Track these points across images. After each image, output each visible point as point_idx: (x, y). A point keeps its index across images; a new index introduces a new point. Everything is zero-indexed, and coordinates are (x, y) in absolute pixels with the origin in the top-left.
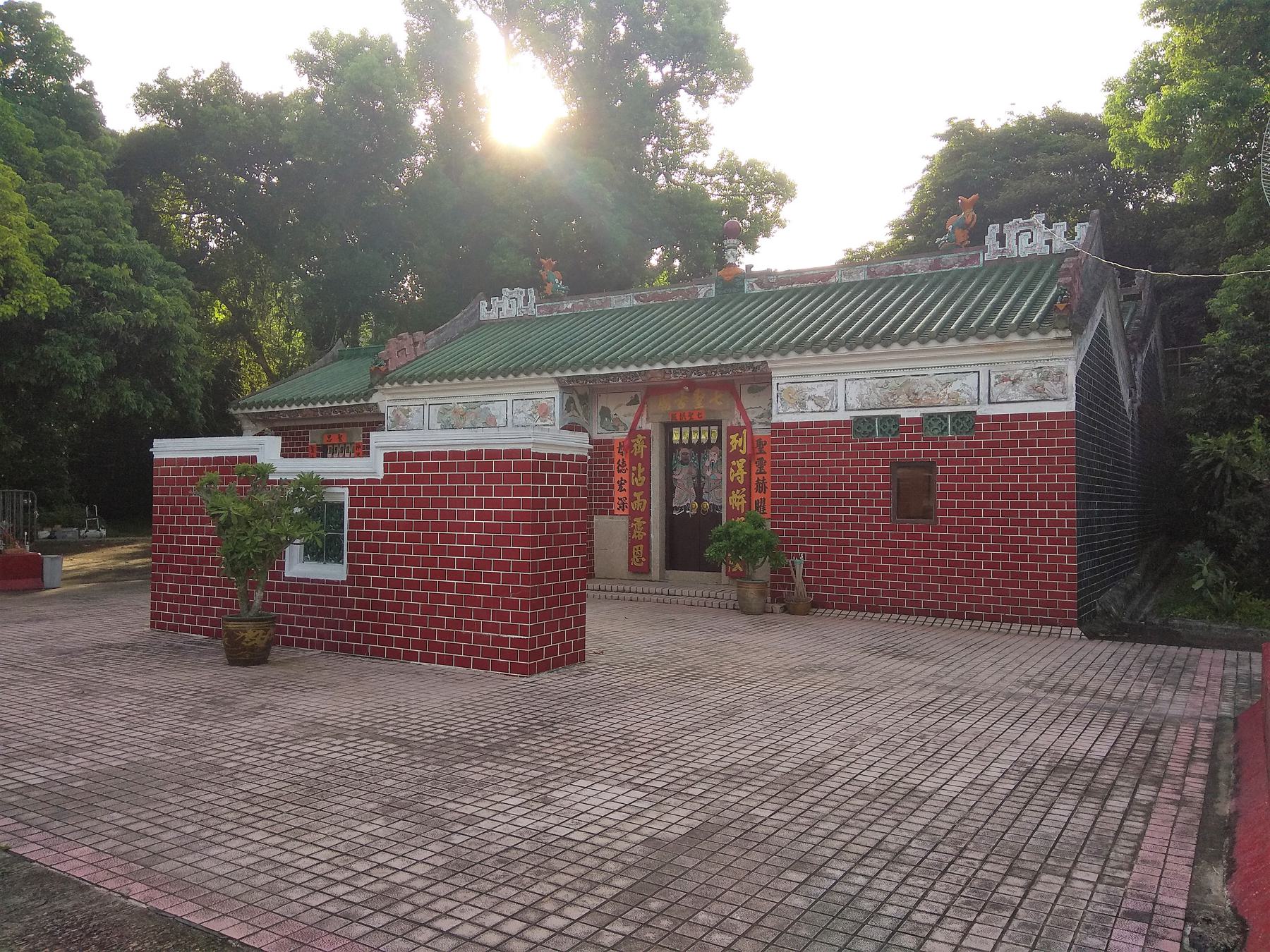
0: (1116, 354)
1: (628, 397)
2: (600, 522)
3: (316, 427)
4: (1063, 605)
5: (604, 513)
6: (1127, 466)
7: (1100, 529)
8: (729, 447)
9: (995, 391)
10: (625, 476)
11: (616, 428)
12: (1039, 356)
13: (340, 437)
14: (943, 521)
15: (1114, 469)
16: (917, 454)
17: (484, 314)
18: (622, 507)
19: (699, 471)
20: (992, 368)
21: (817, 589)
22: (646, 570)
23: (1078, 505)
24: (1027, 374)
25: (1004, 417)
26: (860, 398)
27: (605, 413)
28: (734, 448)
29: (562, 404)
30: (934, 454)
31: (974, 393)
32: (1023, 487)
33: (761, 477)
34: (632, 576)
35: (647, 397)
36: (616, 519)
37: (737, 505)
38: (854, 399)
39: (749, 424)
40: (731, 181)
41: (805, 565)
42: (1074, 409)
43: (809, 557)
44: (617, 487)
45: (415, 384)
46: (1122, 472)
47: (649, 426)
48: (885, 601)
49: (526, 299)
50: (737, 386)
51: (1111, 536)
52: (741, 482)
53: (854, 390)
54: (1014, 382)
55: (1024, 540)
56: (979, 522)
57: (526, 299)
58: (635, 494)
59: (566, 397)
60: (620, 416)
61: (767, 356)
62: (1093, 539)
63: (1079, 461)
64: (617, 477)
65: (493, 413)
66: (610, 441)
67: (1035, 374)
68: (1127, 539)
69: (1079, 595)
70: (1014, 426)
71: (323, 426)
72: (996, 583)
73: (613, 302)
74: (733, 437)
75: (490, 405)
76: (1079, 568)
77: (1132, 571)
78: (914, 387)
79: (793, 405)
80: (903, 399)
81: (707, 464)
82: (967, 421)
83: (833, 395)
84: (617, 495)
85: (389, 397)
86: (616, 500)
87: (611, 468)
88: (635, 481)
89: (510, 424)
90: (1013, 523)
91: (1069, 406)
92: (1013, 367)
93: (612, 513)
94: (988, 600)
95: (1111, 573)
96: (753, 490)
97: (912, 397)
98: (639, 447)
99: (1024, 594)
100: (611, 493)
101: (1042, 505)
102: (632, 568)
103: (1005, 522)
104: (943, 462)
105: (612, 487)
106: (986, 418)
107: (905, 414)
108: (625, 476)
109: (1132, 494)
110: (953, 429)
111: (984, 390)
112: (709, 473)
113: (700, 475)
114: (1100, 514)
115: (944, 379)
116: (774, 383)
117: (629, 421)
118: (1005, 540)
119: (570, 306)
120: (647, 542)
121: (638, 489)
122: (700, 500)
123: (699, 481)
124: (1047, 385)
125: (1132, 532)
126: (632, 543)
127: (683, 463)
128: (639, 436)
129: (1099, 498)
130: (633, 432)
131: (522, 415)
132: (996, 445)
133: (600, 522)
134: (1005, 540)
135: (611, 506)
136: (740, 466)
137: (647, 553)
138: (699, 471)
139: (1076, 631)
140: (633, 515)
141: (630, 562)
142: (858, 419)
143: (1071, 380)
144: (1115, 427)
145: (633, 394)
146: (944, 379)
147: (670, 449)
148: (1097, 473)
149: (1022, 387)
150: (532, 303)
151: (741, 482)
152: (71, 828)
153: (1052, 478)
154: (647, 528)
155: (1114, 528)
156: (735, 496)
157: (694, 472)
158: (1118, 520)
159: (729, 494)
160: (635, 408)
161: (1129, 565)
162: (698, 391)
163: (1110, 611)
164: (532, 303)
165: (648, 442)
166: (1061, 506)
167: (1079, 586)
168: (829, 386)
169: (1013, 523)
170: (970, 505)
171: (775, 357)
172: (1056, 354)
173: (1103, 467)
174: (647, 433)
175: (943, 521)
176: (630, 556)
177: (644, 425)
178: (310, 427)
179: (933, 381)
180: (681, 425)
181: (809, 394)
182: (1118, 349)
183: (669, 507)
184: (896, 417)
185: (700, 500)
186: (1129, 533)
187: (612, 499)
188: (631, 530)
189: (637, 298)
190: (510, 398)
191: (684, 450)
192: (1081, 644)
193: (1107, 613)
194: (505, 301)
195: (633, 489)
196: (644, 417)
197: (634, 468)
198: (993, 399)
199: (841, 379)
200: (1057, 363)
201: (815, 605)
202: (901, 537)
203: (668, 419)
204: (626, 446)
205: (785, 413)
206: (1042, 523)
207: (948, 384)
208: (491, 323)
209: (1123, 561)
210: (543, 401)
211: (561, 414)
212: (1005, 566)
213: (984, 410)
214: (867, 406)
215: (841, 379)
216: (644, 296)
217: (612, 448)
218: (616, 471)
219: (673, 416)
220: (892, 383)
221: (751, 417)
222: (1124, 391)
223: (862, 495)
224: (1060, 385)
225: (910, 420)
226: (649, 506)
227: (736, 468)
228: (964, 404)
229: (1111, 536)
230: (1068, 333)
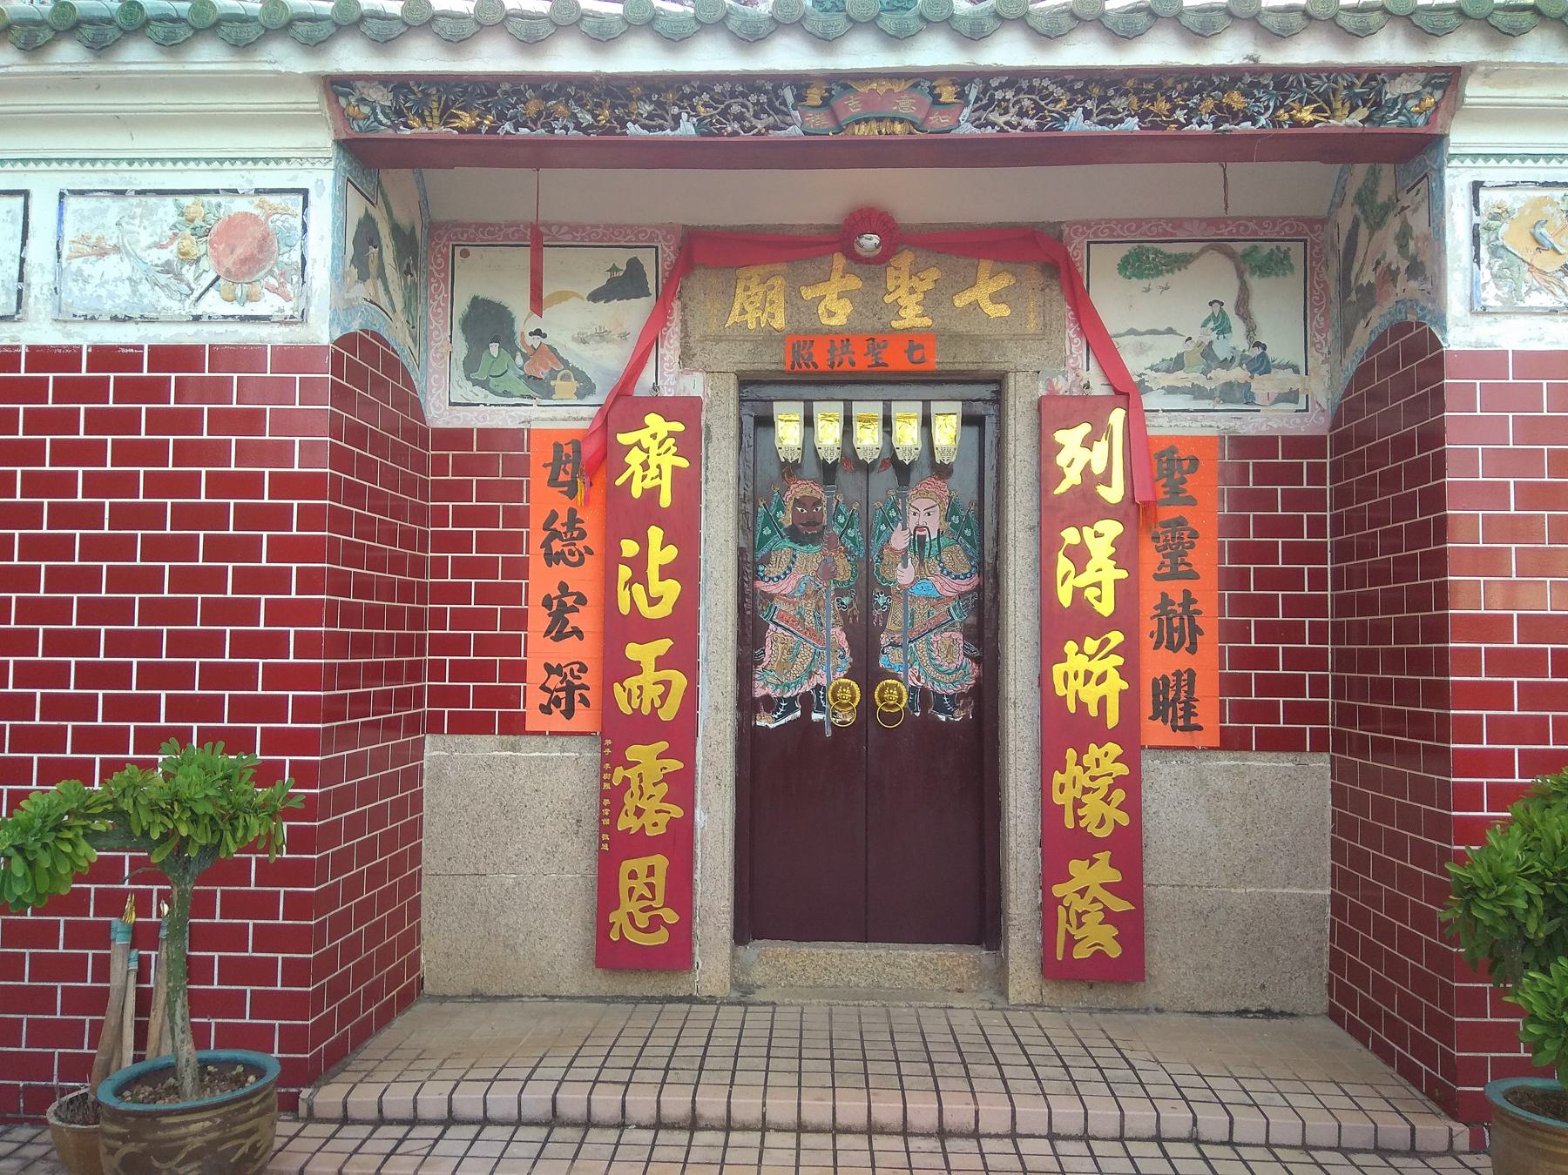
1: (596, 268)
8: (1047, 472)
10: (583, 579)
11: (540, 387)
18: (565, 699)
22: (677, 954)
27: (487, 323)
28: (1073, 478)
33: (1175, 590)
34: (602, 983)
36: (529, 751)
37: (1091, 695)
39: (1126, 393)
44: (539, 619)
47: (694, 385)
50: (1076, 249)
52: (1106, 608)
58: (633, 651)
64: (541, 581)
66: (513, 437)
74: (1070, 439)
81: (900, 540)
84: (539, 650)
86: (536, 674)
87: (513, 543)
93: (514, 726)
96: (1147, 642)
102: (611, 954)
105: (519, 620)
108: (583, 579)
112: (905, 575)
116: (1456, 181)
120: (679, 843)
121: (647, 630)
122: (867, 671)
123: (869, 602)
126: (615, 848)
127: (795, 535)
128: (654, 421)
131: (113, 266)
137: (681, 889)
140: (620, 732)
141: (603, 926)
145: (621, 258)
147: (763, 479)
151: (1106, 608)
154: (682, 787)
156: (1075, 659)
157: (844, 569)
160: (633, 313)
162: (905, 259)
174: (684, 409)
176: (606, 896)
177: (668, 376)
183: (747, 704)
185: (867, 671)
188: (613, 798)
196: (670, 351)
197: (629, 548)
203: (771, 360)
205: (1513, 310)
210: (240, 205)
217: (520, 466)
221: (1135, 364)
223: (152, 612)
227: (1080, 556)
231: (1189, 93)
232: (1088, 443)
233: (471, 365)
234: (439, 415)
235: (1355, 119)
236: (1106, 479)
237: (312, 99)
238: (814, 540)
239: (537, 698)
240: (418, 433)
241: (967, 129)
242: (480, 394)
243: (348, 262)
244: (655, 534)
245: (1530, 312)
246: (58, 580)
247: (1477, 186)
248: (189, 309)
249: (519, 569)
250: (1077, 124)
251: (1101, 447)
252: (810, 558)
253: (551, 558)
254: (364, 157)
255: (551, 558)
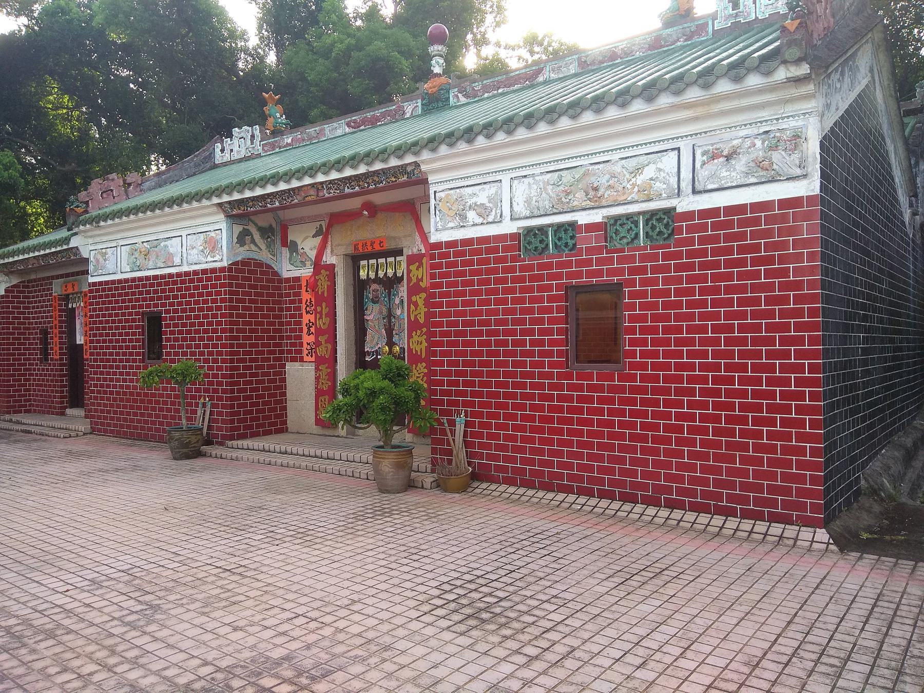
0: (890, 147)
1: (312, 228)
2: (292, 368)
3: (58, 277)
4: (801, 493)
5: (294, 360)
6: (908, 300)
7: (867, 373)
9: (702, 174)
11: (303, 264)
12: (765, 114)
13: (73, 286)
14: (633, 366)
15: (889, 294)
16: (599, 273)
17: (219, 158)
19: (389, 310)
20: (698, 141)
21: (481, 456)
23: (824, 340)
24: (748, 143)
25: (714, 212)
26: (528, 201)
28: (414, 280)
29: (230, 237)
30: (620, 272)
31: (673, 181)
32: (742, 315)
35: (329, 226)
38: (521, 205)
40: (532, 53)
41: (467, 424)
42: (817, 191)
43: (474, 414)
44: (305, 329)
45: (102, 223)
46: (900, 297)
48: (560, 476)
49: (253, 136)
50: (417, 206)
51: (885, 379)
52: (422, 321)
53: (522, 190)
54: (728, 158)
55: (743, 394)
56: (680, 367)
57: (253, 136)
59: (238, 229)
60: (307, 250)
61: (416, 154)
62: (854, 387)
63: (825, 272)
64: (306, 318)
65: (171, 250)
67: (758, 143)
68: (908, 381)
69: (826, 478)
70: (728, 224)
71: (61, 276)
72: (704, 456)
73: (327, 132)
75: (169, 243)
76: (827, 437)
77: (914, 418)
78: (593, 179)
79: (453, 218)
80: (579, 198)
81: (397, 301)
82: (664, 220)
83: (496, 200)
85: (91, 241)
86: (305, 345)
87: (299, 309)
88: (320, 323)
89: (185, 262)
90: (728, 367)
91: (810, 187)
92: (727, 136)
93: (302, 360)
94: (694, 481)
95: (883, 429)
97: (592, 193)
98: (323, 285)
99: (744, 473)
100: (300, 337)
101: (770, 341)
102: (319, 422)
103: (717, 368)
104: (632, 283)
105: (301, 330)
106: (689, 215)
107: (583, 218)
109: (915, 326)
110: (647, 235)
111: (686, 174)
113: (390, 315)
114: (865, 351)
115: (632, 163)
117: (312, 254)
118: (716, 393)
119: (289, 141)
123: (390, 322)
124: (776, 156)
125: (915, 371)
127: (374, 302)
129: (867, 330)
130: (318, 265)
131: (195, 251)
132: (703, 253)
133: (292, 368)
134: (716, 393)
135: (300, 352)
136: (421, 303)
138: (389, 310)
139: (822, 535)
140: (319, 361)
141: (316, 415)
142: (529, 231)
143: (813, 147)
144: (891, 239)
146: (632, 163)
147: (359, 287)
148: (861, 294)
149: (740, 164)
150: (257, 140)
151: (422, 321)
152: (98, 599)
153: (784, 300)
155: (889, 369)
158: (894, 359)
159: (410, 336)
161: (909, 413)
163: (882, 488)
164: (257, 140)
165: (332, 277)
166: (799, 341)
167: (827, 463)
168: (491, 190)
169: (728, 367)
170: (667, 342)
171: (426, 155)
172: (790, 109)
173: (872, 287)
175: (633, 366)
177: (329, 258)
178: (53, 278)
179: (617, 168)
180: (368, 257)
181: (471, 201)
182: (893, 141)
184: (573, 225)
186: (909, 373)
187: (301, 345)
188: (317, 379)
189: (348, 125)
190: (184, 233)
191: (374, 286)
192: (828, 561)
193: (874, 492)
194: (235, 141)
195: (319, 332)
196: (328, 250)
198: (699, 187)
199: (506, 178)
200: (793, 123)
201: (475, 477)
202: (580, 388)
203: (350, 250)
204: (312, 285)
206: (771, 368)
207: (638, 170)
208: (225, 164)
209: (902, 409)
211: (230, 248)
212: (718, 432)
213: (687, 204)
214: (536, 213)
215: (506, 178)
216: (355, 121)
217: (300, 287)
218: (304, 312)
219: (356, 247)
220: (567, 177)
222: (903, 198)
224: (796, 157)
225: (591, 227)
226: (335, 351)
228: (659, 197)
229: (885, 379)
230: (805, 69)
231: (366, 178)
232: (417, 269)
233: (290, 259)
234: (286, 275)
235: (405, 178)
236: (422, 280)
237: (215, 209)
238: (377, 302)
239: (305, 352)
240: (280, 281)
241: (327, 195)
242: (292, 267)
243: (235, 240)
244: (324, 305)
245: (447, 229)
246: (730, 328)
247: (435, 192)
248: (205, 260)
249: (301, 316)
250: (347, 191)
251: (421, 269)
252: (376, 307)
253: (307, 312)
254: (232, 218)
255: (307, 312)
